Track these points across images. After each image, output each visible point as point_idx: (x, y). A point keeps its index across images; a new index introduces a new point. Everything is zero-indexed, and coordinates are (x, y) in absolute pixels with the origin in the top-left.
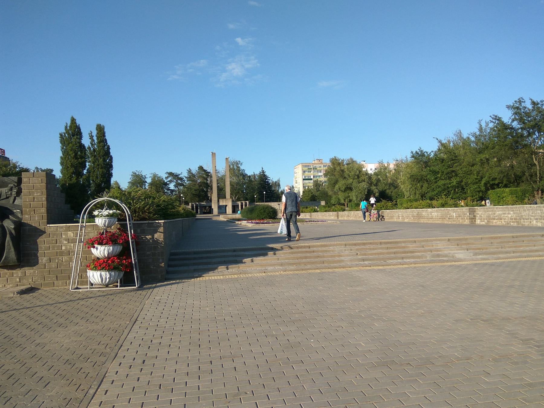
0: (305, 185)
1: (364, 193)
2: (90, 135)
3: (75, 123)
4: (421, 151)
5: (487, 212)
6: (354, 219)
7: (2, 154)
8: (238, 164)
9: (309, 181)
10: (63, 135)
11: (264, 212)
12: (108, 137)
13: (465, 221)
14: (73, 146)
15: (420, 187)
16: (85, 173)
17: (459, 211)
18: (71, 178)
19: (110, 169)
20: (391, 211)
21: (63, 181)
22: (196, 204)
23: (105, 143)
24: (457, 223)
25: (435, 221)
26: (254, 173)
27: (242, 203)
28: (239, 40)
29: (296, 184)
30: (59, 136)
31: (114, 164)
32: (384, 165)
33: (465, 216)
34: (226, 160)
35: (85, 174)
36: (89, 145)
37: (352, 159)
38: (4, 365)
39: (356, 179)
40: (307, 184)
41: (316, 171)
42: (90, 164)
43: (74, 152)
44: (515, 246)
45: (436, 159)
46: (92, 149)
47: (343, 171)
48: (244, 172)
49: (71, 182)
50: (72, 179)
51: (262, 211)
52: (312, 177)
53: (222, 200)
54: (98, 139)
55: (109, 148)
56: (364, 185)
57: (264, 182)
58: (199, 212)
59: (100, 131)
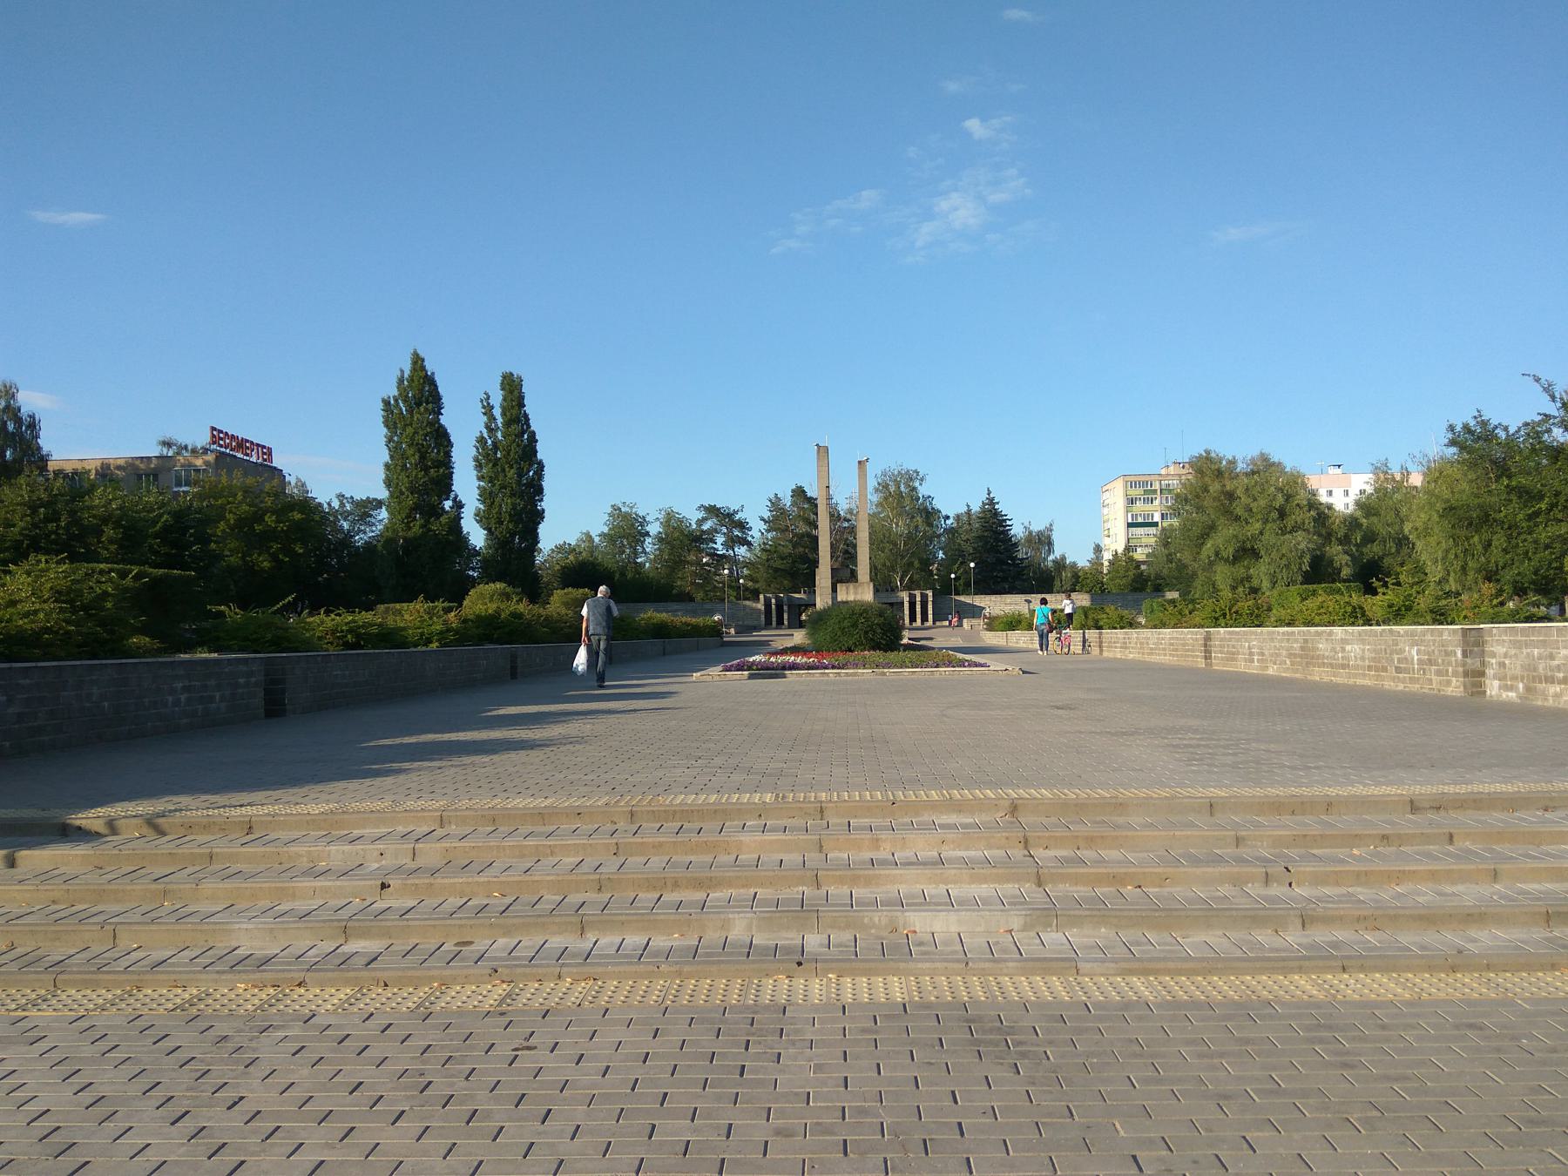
0: (1134, 541)
1: (1300, 568)
2: (485, 404)
3: (423, 368)
4: (1484, 424)
5: (1527, 646)
6: (1137, 655)
7: (265, 460)
8: (911, 479)
9: (1139, 529)
10: (392, 402)
11: (855, 625)
12: (530, 408)
13: (1449, 683)
14: (415, 433)
15: (1479, 547)
16: (447, 508)
17: (1429, 641)
18: (410, 517)
19: (537, 498)
20: (1230, 633)
21: (388, 531)
22: (777, 598)
23: (525, 427)
24: (1424, 690)
25: (1356, 676)
26: (968, 506)
28: (973, 125)
30: (381, 405)
31: (547, 484)
32: (1393, 475)
33: (1449, 664)
34: (859, 468)
35: (448, 512)
37: (1264, 458)
38: (167, 1035)
39: (1274, 521)
41: (1144, 500)
42: (482, 484)
43: (419, 451)
44: (1358, 874)
45: (1533, 450)
46: (489, 442)
47: (1231, 496)
48: (931, 503)
49: (410, 534)
50: (412, 525)
51: (846, 623)
52: (1157, 518)
53: (844, 588)
54: (503, 414)
55: (533, 439)
56: (1302, 542)
58: (786, 622)
59: (511, 392)
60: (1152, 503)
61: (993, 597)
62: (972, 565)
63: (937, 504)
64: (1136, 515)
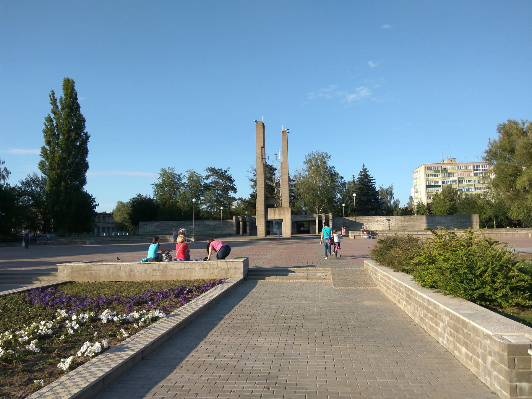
0: (430, 194)
2: (52, 97)
12: (80, 100)
26: (353, 175)
27: (320, 218)
29: (416, 194)
31: (90, 145)
34: (283, 135)
36: (49, 115)
40: (432, 193)
48: (334, 170)
53: (272, 211)
57: (367, 186)
58: (248, 231)
60: (438, 177)
61: (367, 218)
62: (355, 195)
63: (337, 170)
64: (430, 182)
